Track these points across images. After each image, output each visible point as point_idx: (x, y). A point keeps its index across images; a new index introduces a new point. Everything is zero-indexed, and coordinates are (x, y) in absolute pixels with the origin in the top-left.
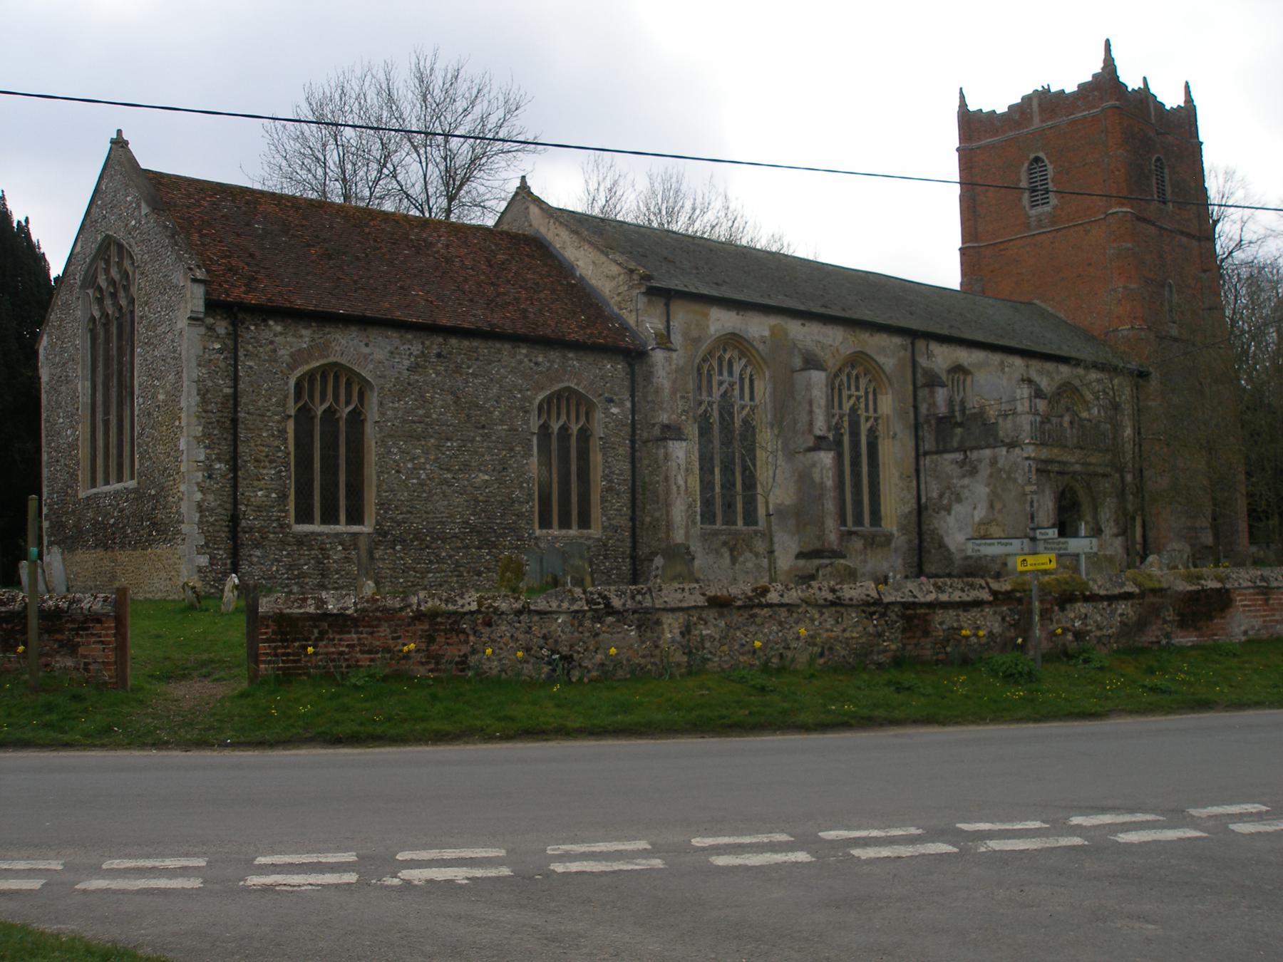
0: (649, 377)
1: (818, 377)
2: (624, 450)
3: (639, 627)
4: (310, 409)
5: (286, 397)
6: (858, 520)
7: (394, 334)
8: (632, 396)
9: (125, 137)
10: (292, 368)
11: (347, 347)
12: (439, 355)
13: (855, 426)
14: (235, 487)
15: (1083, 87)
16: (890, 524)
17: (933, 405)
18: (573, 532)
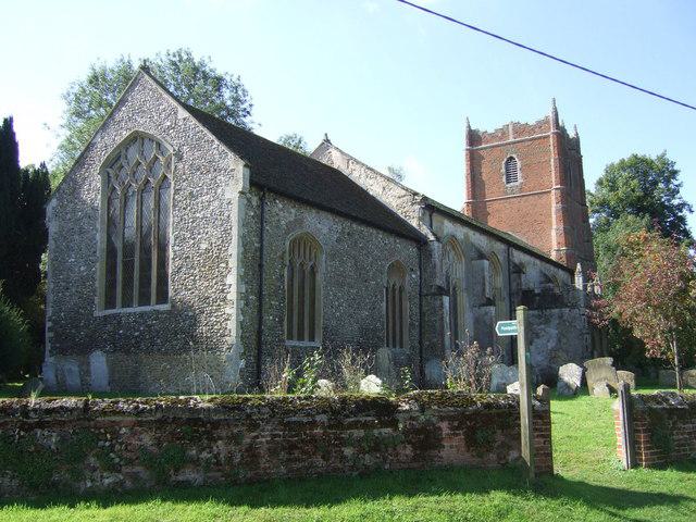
2: (417, 300)
5: (284, 252)
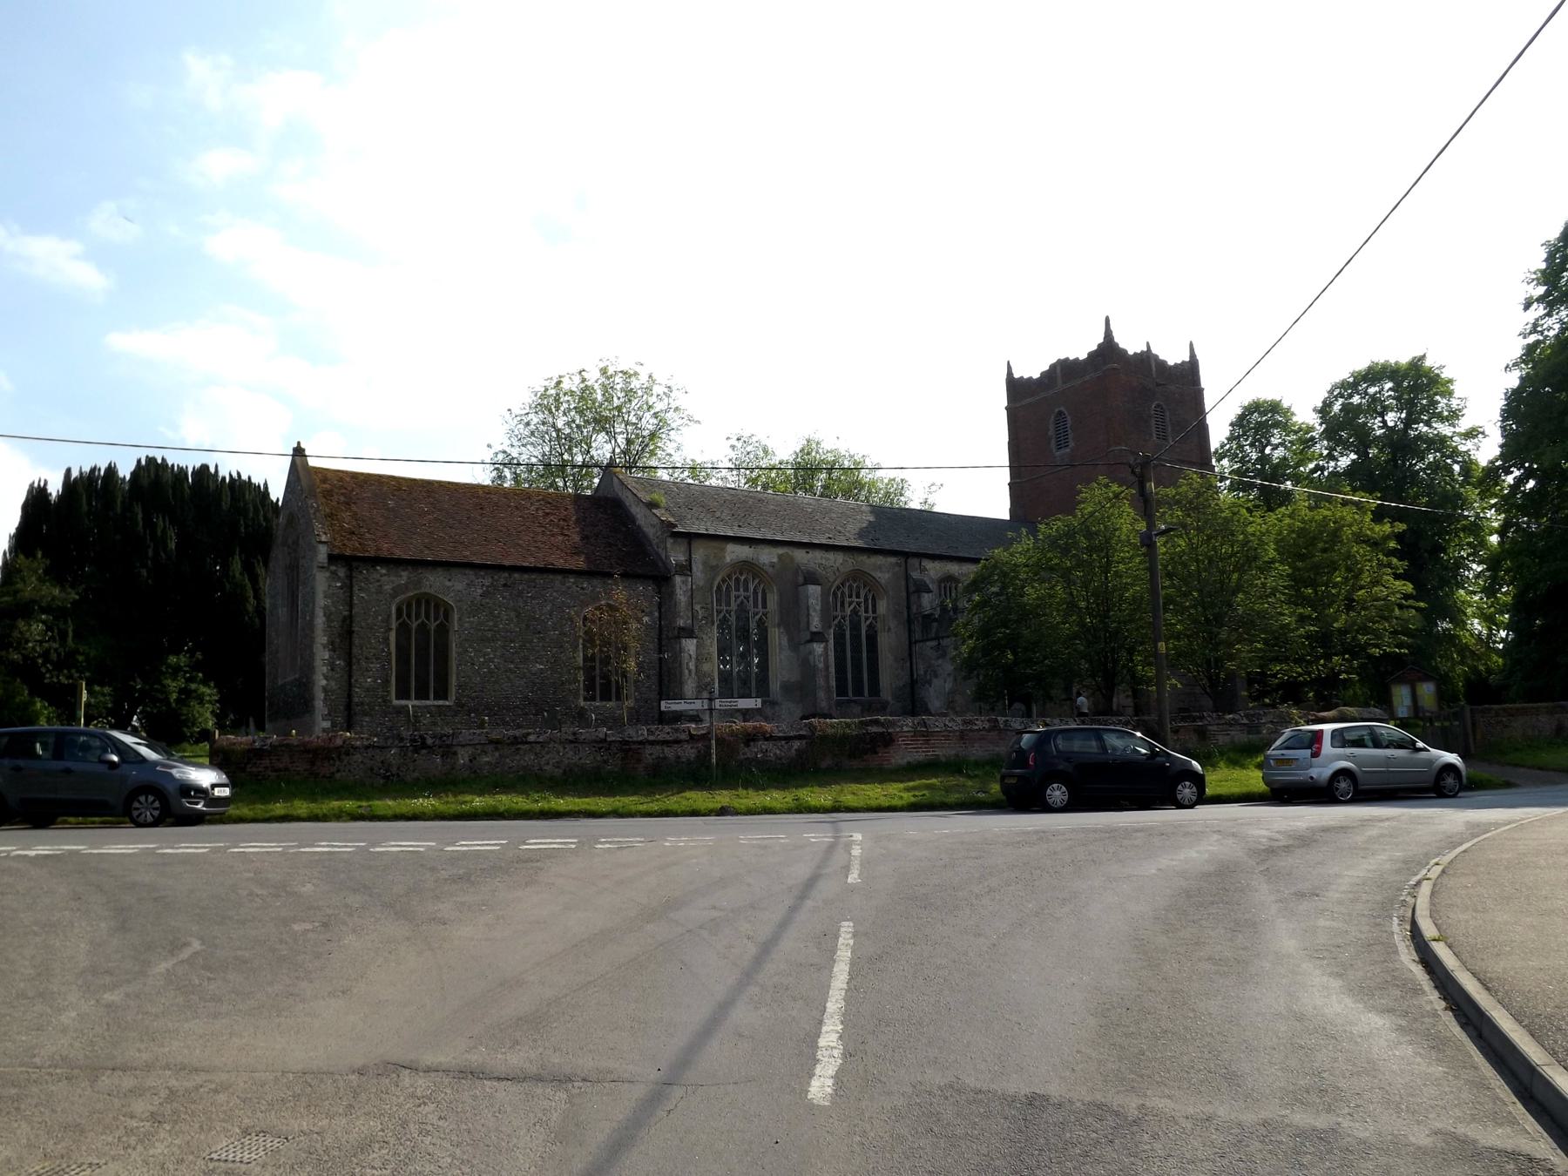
0: (672, 594)
1: (814, 590)
6: (858, 691)
7: (470, 572)
11: (434, 582)
13: (855, 627)
14: (350, 677)
15: (1090, 354)
16: (886, 694)
18: (609, 705)
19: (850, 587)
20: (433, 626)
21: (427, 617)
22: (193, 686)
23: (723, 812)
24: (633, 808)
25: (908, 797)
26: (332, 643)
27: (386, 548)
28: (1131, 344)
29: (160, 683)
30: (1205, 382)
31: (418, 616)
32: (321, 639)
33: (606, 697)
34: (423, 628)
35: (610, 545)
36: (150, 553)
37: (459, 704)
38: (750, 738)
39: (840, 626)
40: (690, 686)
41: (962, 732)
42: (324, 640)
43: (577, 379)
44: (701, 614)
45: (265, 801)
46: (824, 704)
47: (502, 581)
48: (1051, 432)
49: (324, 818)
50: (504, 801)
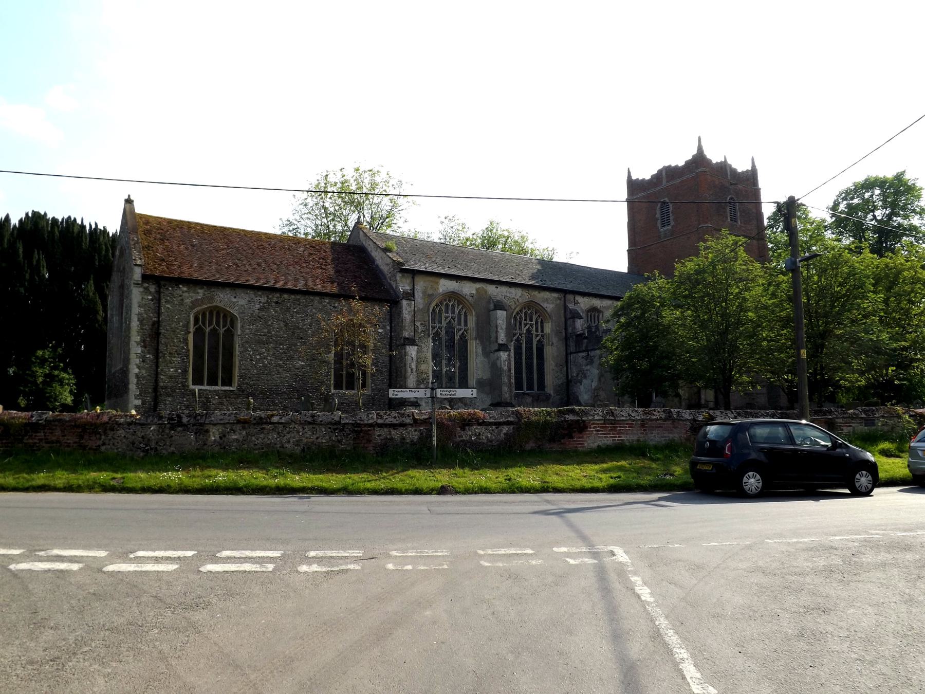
0: (400, 313)
1: (501, 315)
3: (196, 433)
4: (231, 331)
6: (530, 387)
8: (391, 323)
9: (132, 198)
10: (192, 308)
11: (223, 299)
12: (277, 303)
14: (157, 367)
15: (687, 163)
16: (549, 390)
17: (574, 328)
19: (526, 314)
20: (222, 331)
21: (218, 324)
22: (56, 373)
23: (443, 491)
24: (361, 485)
25: (606, 479)
26: (144, 341)
27: (187, 272)
28: (714, 156)
29: (30, 369)
30: (761, 184)
31: (210, 323)
32: (135, 338)
33: (350, 386)
34: (214, 332)
35: (356, 277)
36: (27, 276)
37: (240, 389)
38: (465, 423)
39: (518, 340)
40: (411, 380)
41: (643, 420)
42: (138, 339)
43: (339, 175)
44: (421, 328)
45: (31, 471)
46: (507, 395)
47: (275, 300)
48: (658, 216)
49: (78, 489)
50: (245, 476)
